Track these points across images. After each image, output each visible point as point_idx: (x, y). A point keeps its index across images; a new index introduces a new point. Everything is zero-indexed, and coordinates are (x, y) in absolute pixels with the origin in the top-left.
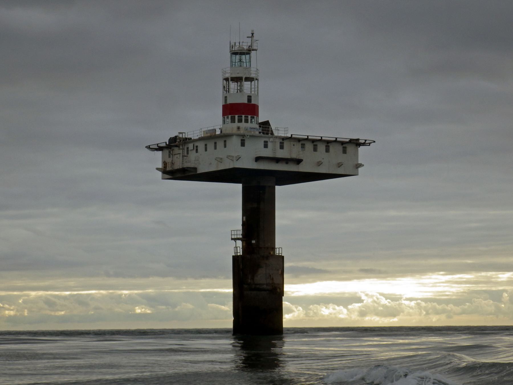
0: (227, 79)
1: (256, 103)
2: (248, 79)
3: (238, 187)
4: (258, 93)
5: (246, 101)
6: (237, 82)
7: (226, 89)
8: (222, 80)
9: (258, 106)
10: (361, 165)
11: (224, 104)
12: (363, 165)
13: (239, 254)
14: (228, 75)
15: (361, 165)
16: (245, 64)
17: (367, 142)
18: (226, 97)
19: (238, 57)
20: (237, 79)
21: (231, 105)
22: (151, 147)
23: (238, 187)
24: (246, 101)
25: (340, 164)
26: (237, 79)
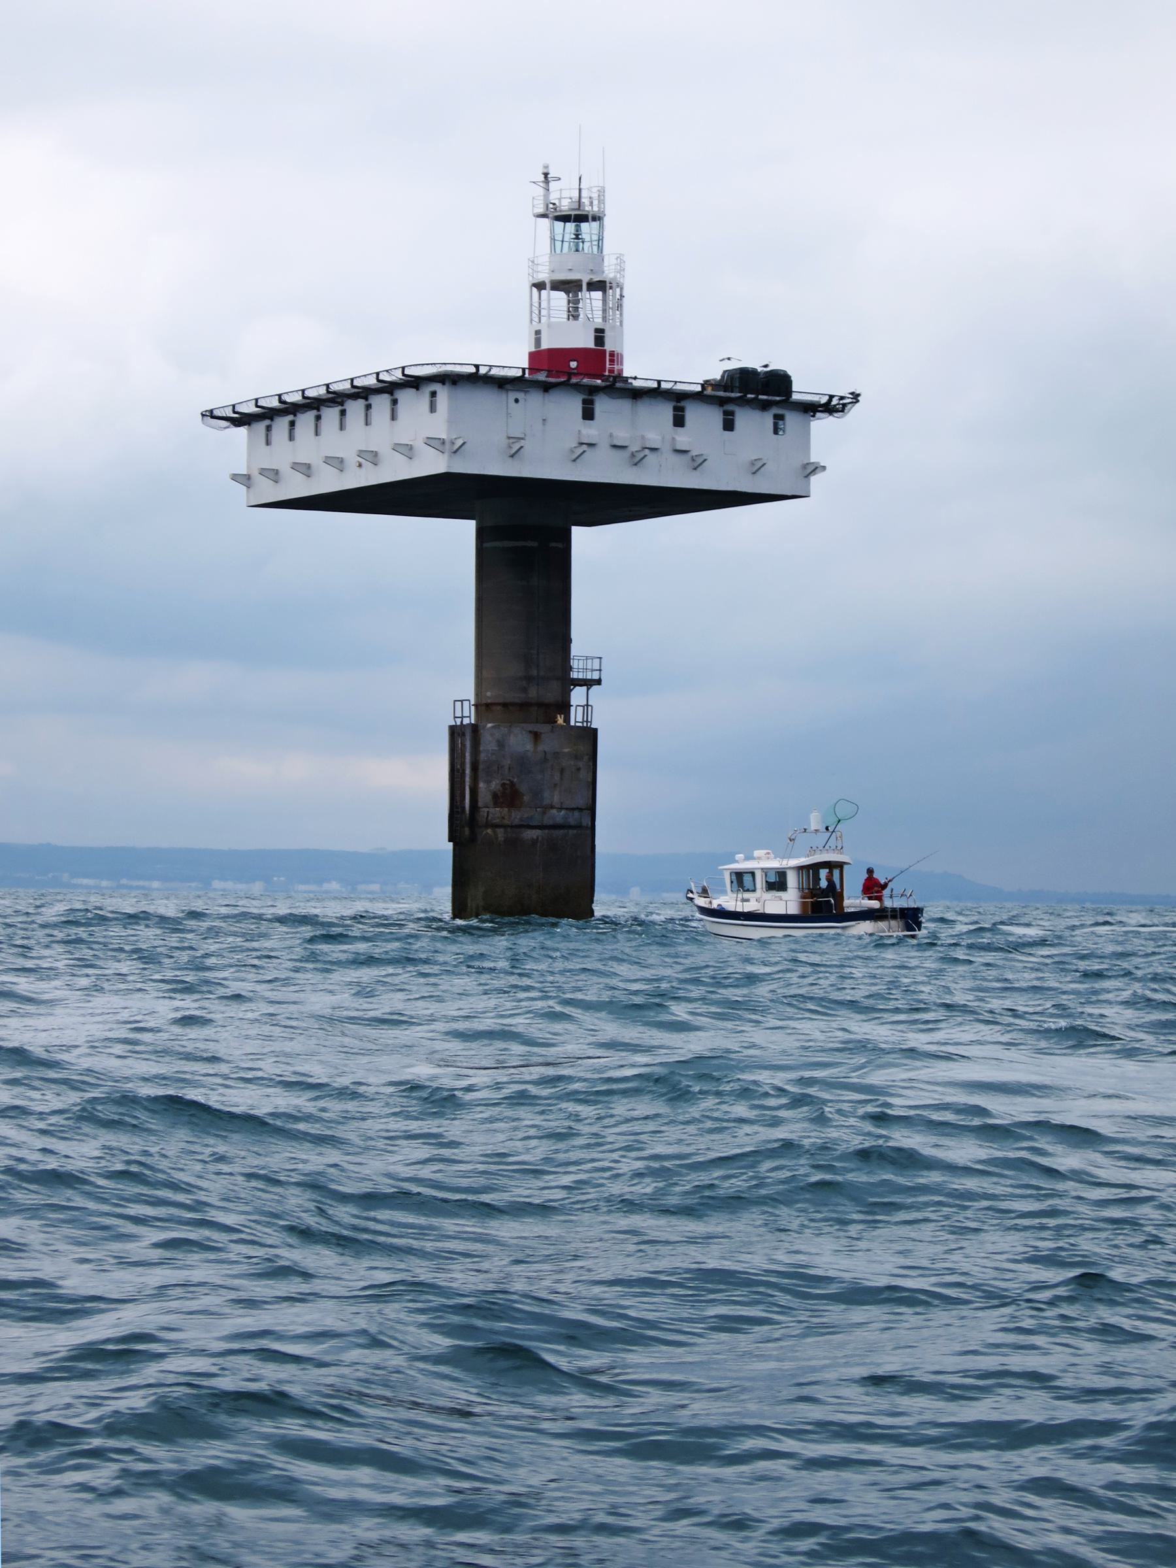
0: (540, 286)
1: (617, 350)
2: (595, 286)
3: (467, 529)
4: (621, 322)
5: (590, 344)
6: (567, 293)
7: (537, 312)
8: (527, 286)
9: (622, 356)
10: (816, 469)
11: (533, 349)
12: (824, 468)
13: (466, 721)
14: (544, 276)
15: (816, 469)
16: (587, 245)
17: (835, 401)
18: (538, 332)
19: (571, 227)
20: (569, 287)
21: (552, 352)
22: (216, 413)
23: (467, 529)
24: (590, 344)
25: (759, 464)
26: (569, 287)
